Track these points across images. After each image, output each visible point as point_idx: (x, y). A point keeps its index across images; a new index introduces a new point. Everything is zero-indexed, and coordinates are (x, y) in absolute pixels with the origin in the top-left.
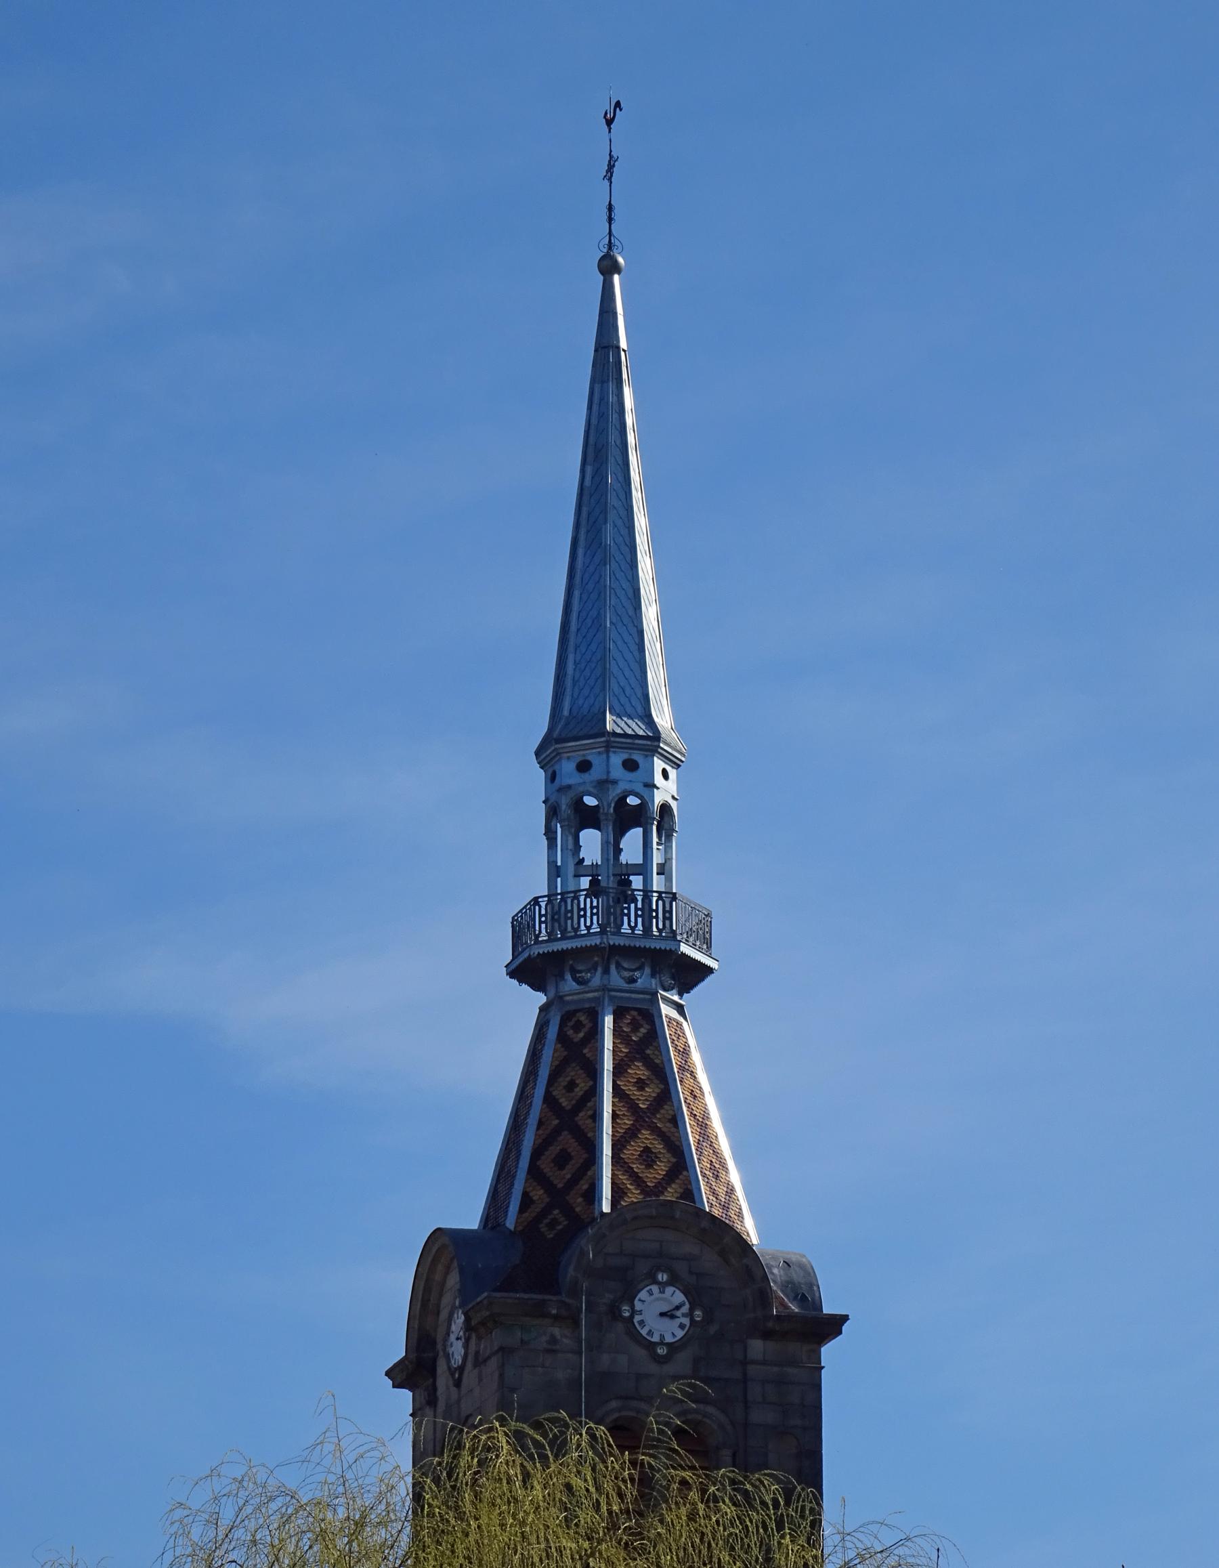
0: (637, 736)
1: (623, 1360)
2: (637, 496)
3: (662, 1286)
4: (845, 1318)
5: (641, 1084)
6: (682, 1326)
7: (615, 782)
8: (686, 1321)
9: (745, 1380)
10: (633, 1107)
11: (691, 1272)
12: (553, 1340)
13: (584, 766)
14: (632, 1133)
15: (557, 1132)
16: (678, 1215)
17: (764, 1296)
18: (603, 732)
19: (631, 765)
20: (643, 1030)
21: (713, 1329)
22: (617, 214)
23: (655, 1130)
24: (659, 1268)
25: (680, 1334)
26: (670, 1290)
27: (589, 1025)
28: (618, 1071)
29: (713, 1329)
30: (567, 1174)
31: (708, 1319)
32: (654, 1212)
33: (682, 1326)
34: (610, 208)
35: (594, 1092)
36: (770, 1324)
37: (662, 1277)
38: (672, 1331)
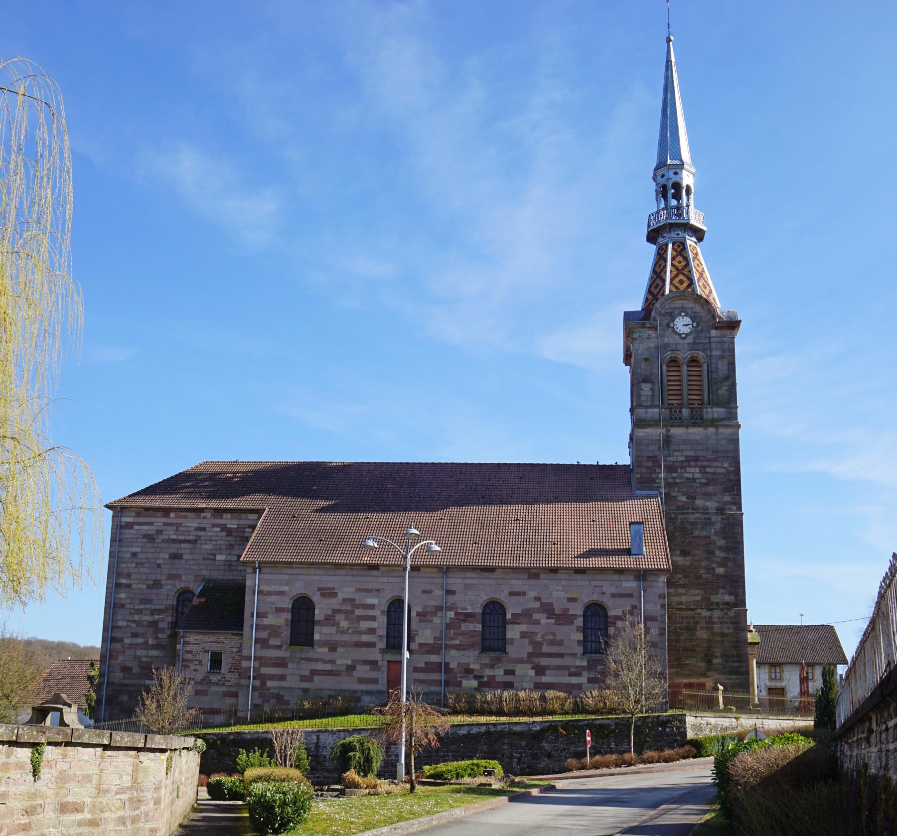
0: (677, 165)
1: (671, 339)
2: (674, 68)
3: (683, 317)
4: (105, 506)
5: (680, 262)
6: (690, 328)
7: (671, 179)
8: (691, 326)
9: (710, 342)
10: (677, 269)
11: (692, 312)
12: (650, 335)
13: (663, 176)
14: (677, 276)
15: (656, 279)
16: (686, 295)
17: (714, 317)
18: (667, 165)
19: (676, 173)
20: (681, 248)
21: (699, 328)
22: (670, 26)
23: (684, 274)
24: (682, 312)
25: (689, 330)
26: (685, 318)
27: (665, 248)
28: (673, 259)
29: (699, 328)
30: (658, 290)
31: (698, 325)
32: (679, 295)
33: (690, 328)
34: (669, 25)
35: (665, 266)
36: (716, 325)
37: (683, 314)
38: (687, 330)
